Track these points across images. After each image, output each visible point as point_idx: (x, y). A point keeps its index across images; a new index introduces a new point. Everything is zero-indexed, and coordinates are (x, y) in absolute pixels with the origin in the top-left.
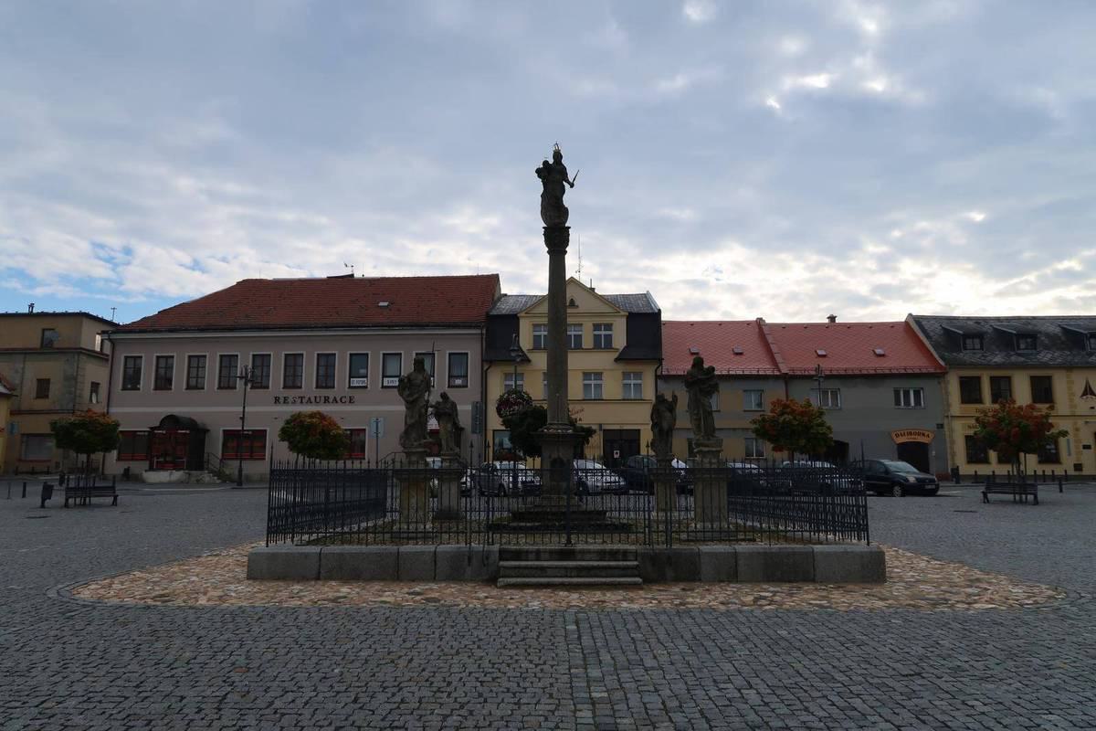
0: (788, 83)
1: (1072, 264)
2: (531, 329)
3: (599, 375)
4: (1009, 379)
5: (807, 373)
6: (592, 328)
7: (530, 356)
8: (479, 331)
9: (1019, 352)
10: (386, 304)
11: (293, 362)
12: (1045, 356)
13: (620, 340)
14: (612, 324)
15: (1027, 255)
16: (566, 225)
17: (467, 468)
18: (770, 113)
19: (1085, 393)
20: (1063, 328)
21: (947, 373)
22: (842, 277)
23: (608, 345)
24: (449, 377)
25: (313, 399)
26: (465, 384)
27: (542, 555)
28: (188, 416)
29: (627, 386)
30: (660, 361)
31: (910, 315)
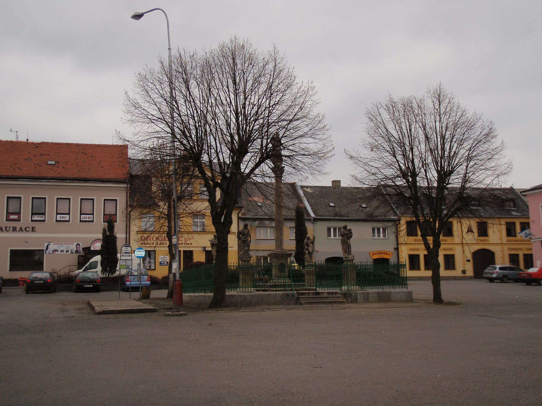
8: (125, 185)
10: (53, 163)
19: (468, 231)
24: (20, 213)
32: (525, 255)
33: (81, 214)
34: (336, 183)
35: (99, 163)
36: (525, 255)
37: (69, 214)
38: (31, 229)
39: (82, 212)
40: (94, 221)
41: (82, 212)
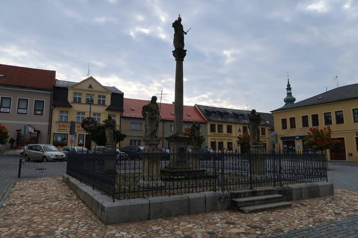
0: (138, 29)
1: (205, 96)
2: (73, 95)
4: (222, 125)
5: (169, 120)
6: (98, 97)
7: (72, 105)
8: (50, 93)
9: (224, 118)
12: (230, 120)
13: (108, 102)
14: (105, 96)
15: (195, 92)
16: (184, 49)
18: (131, 37)
20: (233, 112)
21: (207, 123)
22: (147, 91)
24: (43, 111)
26: (42, 114)
27: (246, 195)
31: (196, 104)
32: (219, 142)
33: (18, 108)
34: (254, 111)
36: (219, 142)
37: (10, 108)
39: (19, 108)
40: (28, 113)
41: (19, 108)
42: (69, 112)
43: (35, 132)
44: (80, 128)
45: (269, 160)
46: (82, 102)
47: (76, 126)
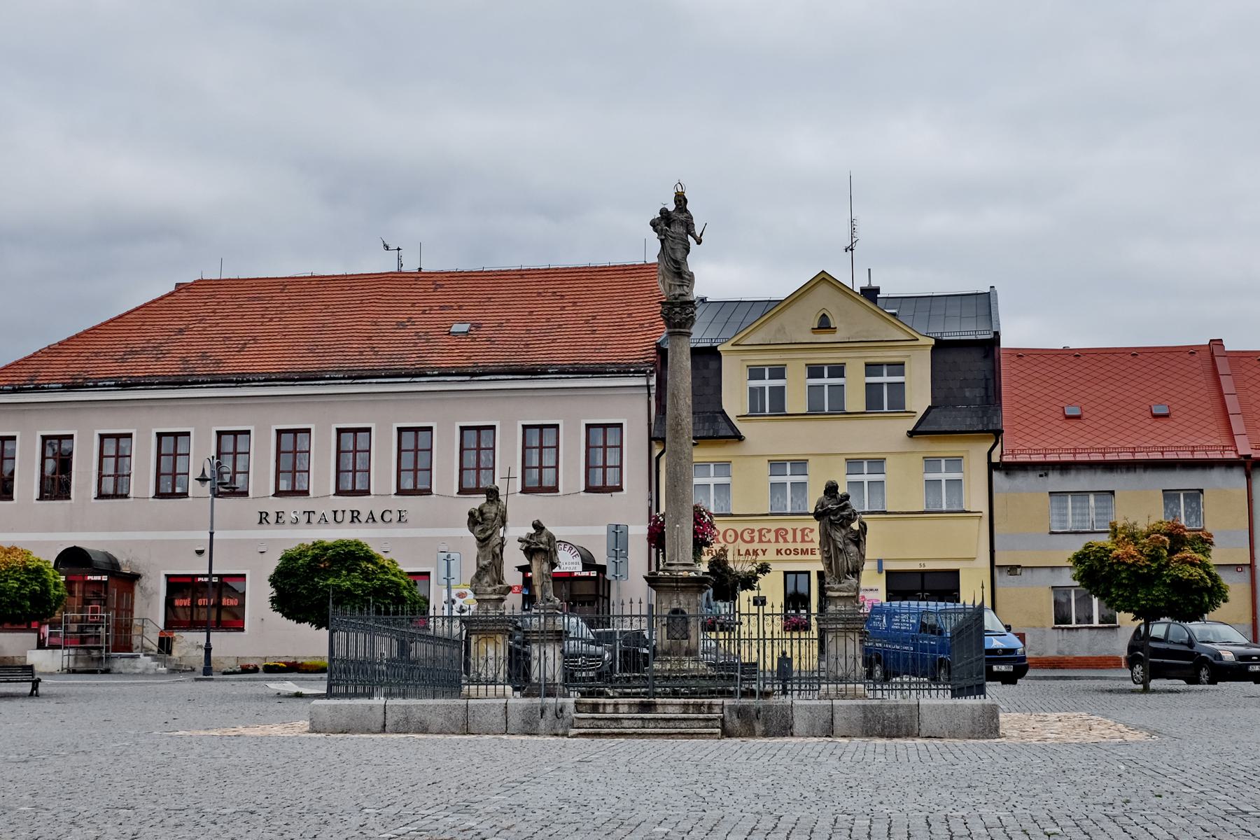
3: (877, 463)
7: (742, 427)
8: (642, 381)
10: (465, 327)
11: (291, 445)
13: (919, 398)
17: (636, 653)
23: (898, 404)
25: (330, 517)
28: (101, 548)
29: (933, 485)
30: (998, 433)
35: (587, 322)
38: (395, 516)
42: (733, 466)
43: (587, 574)
44: (785, 541)
45: (549, 675)
46: (849, 408)
47: (769, 531)
